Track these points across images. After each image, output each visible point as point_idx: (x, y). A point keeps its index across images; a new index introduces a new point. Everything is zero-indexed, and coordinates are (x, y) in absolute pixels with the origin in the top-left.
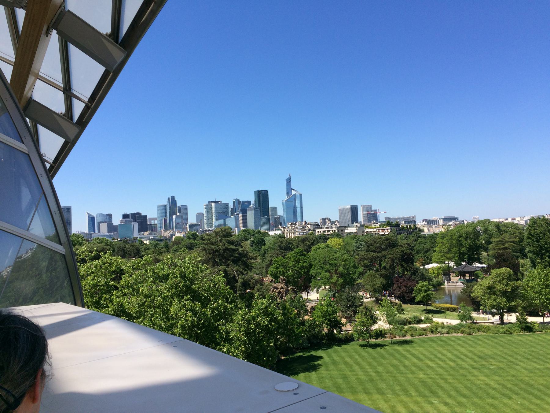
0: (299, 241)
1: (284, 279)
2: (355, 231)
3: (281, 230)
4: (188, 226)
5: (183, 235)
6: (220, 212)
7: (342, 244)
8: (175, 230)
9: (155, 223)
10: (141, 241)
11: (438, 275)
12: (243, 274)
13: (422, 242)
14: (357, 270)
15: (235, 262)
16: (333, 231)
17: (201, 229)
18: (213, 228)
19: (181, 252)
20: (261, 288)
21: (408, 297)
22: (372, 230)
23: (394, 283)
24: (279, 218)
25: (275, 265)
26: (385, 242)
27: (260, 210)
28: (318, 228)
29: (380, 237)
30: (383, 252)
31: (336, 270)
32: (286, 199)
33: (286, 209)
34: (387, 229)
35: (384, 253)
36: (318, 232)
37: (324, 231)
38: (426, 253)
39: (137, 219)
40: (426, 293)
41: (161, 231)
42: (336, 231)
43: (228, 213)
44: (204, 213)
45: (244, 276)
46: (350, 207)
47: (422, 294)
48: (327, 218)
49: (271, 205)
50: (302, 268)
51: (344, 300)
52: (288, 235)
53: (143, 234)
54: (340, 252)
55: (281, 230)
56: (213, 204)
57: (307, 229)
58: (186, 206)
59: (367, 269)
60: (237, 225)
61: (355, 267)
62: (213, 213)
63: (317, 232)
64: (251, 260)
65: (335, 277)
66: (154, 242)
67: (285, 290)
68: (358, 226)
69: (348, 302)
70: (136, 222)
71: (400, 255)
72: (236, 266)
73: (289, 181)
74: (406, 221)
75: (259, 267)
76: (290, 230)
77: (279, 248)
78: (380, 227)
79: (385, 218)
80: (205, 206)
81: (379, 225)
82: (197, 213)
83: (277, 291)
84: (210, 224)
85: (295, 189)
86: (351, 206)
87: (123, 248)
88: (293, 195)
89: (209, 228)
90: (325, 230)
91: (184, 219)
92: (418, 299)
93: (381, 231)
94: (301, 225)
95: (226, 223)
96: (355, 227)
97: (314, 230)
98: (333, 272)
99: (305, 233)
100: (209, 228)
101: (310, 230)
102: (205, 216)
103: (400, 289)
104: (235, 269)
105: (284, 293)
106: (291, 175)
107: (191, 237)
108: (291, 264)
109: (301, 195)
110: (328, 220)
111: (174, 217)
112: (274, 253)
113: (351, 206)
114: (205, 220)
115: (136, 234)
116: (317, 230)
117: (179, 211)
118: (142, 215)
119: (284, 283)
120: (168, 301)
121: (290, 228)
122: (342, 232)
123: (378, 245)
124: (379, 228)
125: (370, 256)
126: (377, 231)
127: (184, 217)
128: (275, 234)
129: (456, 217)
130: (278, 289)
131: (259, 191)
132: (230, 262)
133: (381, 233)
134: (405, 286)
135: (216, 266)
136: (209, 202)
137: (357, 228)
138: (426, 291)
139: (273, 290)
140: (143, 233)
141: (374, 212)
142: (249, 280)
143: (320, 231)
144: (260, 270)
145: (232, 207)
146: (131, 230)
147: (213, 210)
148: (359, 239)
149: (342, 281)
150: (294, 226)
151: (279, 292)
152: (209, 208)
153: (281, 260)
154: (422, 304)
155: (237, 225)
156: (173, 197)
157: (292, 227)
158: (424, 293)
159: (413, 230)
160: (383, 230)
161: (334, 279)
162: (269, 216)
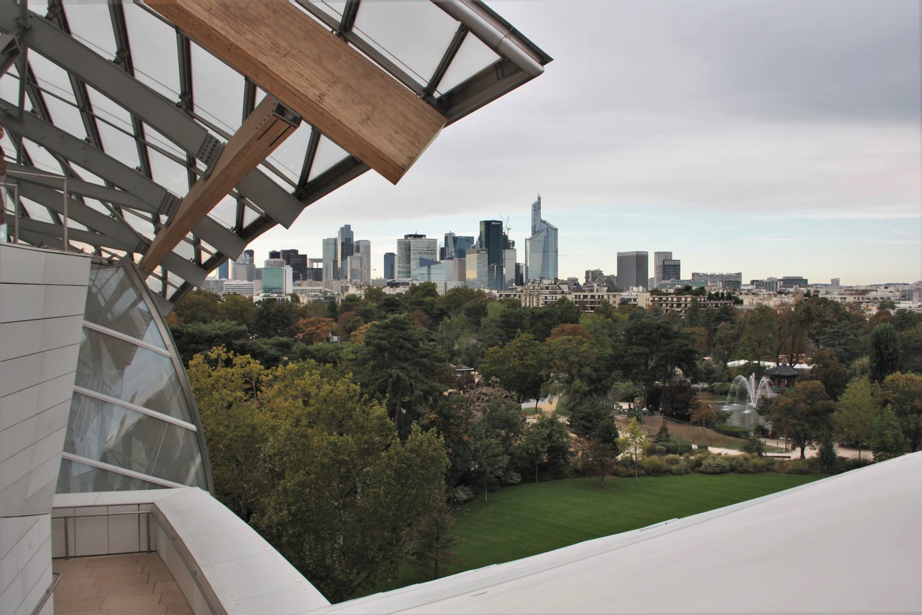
9: (319, 267)
37: (585, 297)
52: (528, 299)
58: (368, 242)
73: (537, 208)
74: (726, 282)
82: (387, 254)
90: (586, 294)
91: (365, 263)
115: (289, 287)
120: (290, 403)
122: (614, 299)
129: (804, 278)
141: (524, 281)
145: (443, 246)
146: (281, 275)
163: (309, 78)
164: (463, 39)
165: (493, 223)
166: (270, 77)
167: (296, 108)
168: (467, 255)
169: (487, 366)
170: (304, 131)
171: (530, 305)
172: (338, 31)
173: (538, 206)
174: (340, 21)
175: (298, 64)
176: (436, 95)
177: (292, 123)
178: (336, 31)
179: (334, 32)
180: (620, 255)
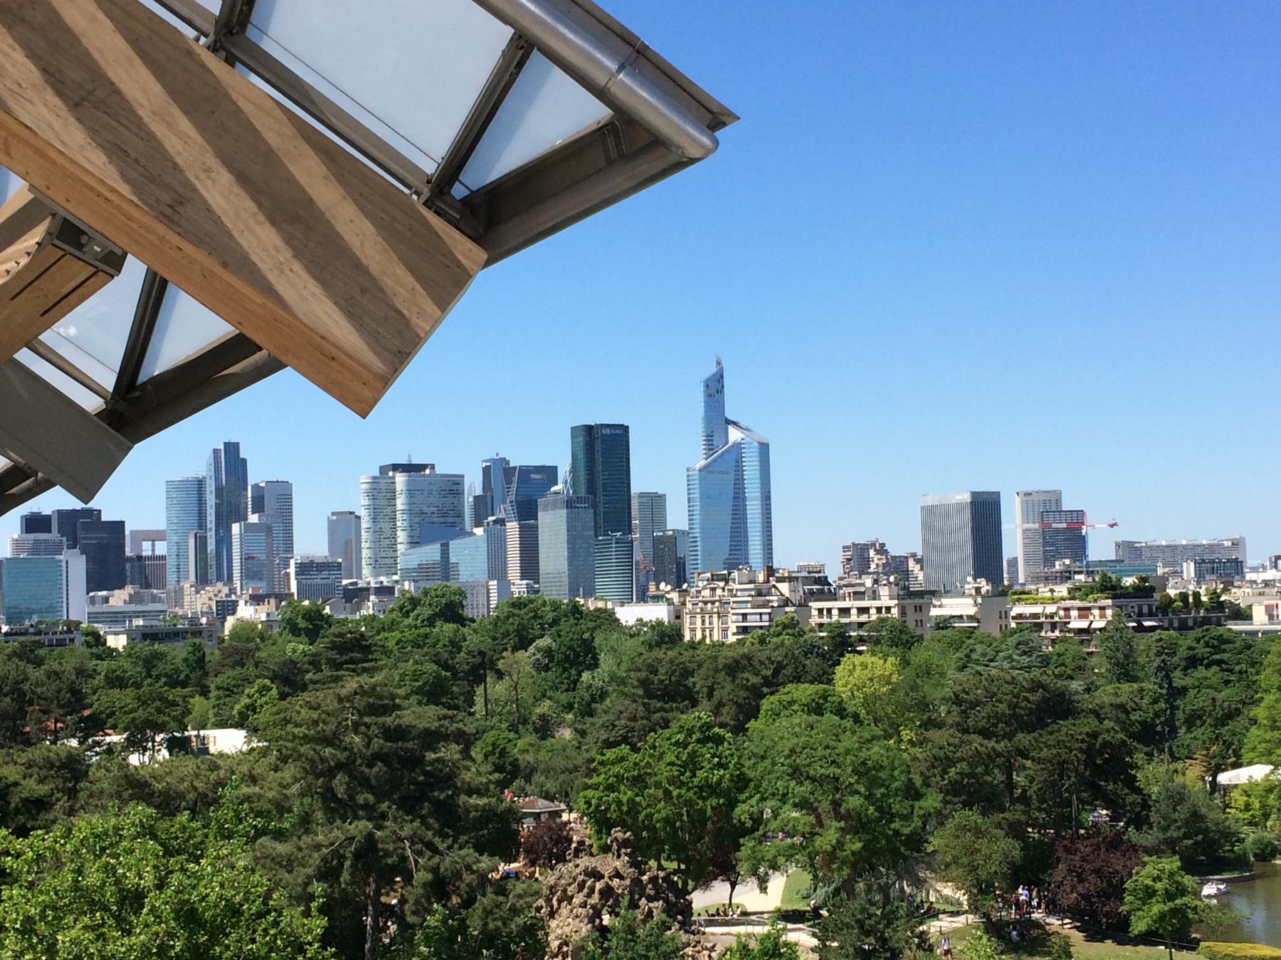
0: (717, 671)
1: (628, 839)
2: (972, 611)
3: (670, 602)
4: (292, 570)
5: (268, 615)
6: (426, 509)
7: (894, 678)
8: (237, 583)
9: (158, 553)
10: (96, 635)
11: (1266, 816)
12: (435, 850)
13: (1208, 682)
14: (917, 804)
15: (409, 805)
16: (879, 610)
17: (345, 582)
18: (395, 578)
19: (249, 697)
20: (498, 906)
21: (1107, 915)
22: (1037, 609)
23: (1058, 860)
24: (672, 541)
25: (603, 776)
26: (1026, 699)
27: (594, 507)
28: (821, 596)
29: (1008, 678)
30: (1020, 736)
31: (836, 804)
32: (703, 463)
33: (702, 506)
34: (1102, 608)
35: (1023, 739)
36: (820, 611)
37: (845, 611)
38: (1223, 725)
39: (81, 534)
40: (1171, 905)
41: (182, 589)
42: (895, 611)
43: (460, 515)
44: (363, 513)
45: (437, 859)
46: (967, 498)
47: (1157, 908)
48: (873, 545)
49: (639, 484)
50: (709, 789)
51: (848, 926)
52: (699, 621)
53: (106, 600)
54: (854, 732)
55: (670, 602)
56: (400, 479)
57: (774, 600)
58: (286, 486)
59: (957, 799)
60: (497, 569)
61: (912, 793)
62: (399, 516)
63: (815, 613)
64: (470, 796)
65: (832, 831)
66: (145, 648)
67: (628, 882)
68: (983, 591)
69: (863, 937)
70: (77, 551)
71: (1081, 750)
72: (412, 821)
73: (715, 388)
74: (1203, 561)
75: (559, 762)
76: (706, 603)
77: (640, 692)
78: (1073, 598)
79: (1118, 545)
80: (364, 486)
81: (1070, 591)
82: (333, 514)
83: (598, 886)
84: (384, 562)
85: (742, 424)
86: (974, 494)
87: (17, 683)
88: (733, 446)
89: (382, 578)
92: (1139, 926)
93: (1074, 613)
94: (750, 582)
95: (453, 560)
96: (971, 595)
97: (803, 605)
98: (825, 806)
99: (766, 617)
100: (382, 578)
101: (787, 602)
102: (365, 524)
103: (1081, 880)
104: (407, 831)
105: (622, 895)
106: (724, 364)
107: (302, 624)
108: (664, 772)
109: (764, 448)
110: (878, 552)
111: (236, 528)
112: (621, 712)
113: (974, 494)
114: (364, 545)
116: (815, 605)
117: (258, 507)
118: (104, 518)
119: (626, 854)
121: (707, 593)
122: (918, 616)
123: (1002, 707)
124: (1068, 603)
125: (965, 751)
126: (1062, 613)
127: (278, 529)
128: (641, 620)
130: (603, 877)
131: (589, 429)
132: (389, 807)
133: (1077, 624)
134: (1097, 872)
135: (339, 822)
136: (384, 470)
137: (979, 600)
138: (1170, 896)
139: (584, 882)
140: (104, 593)
141: (1064, 525)
142: (457, 875)
143: (829, 611)
144: (563, 777)
145: (479, 492)
146: (56, 579)
147: (401, 503)
148: (974, 656)
149: (858, 845)
150: (722, 584)
151: (607, 892)
152: (380, 492)
153: (622, 759)
154: (1162, 944)
155: (497, 569)
156: (232, 449)
157: (713, 589)
158: (1164, 902)
159: (1207, 610)
160: (1084, 612)
161: (829, 837)
162: (629, 530)
163: (143, 161)
164: (520, 65)
165: (608, 431)
166: (43, 155)
167: (108, 231)
168: (540, 514)
169: (598, 794)
170: (134, 273)
171: (704, 637)
172: (212, 37)
173: (714, 385)
174: (217, 14)
175: (114, 124)
176: (458, 191)
177: (102, 266)
178: (206, 36)
179: (203, 40)
180: (980, 499)
